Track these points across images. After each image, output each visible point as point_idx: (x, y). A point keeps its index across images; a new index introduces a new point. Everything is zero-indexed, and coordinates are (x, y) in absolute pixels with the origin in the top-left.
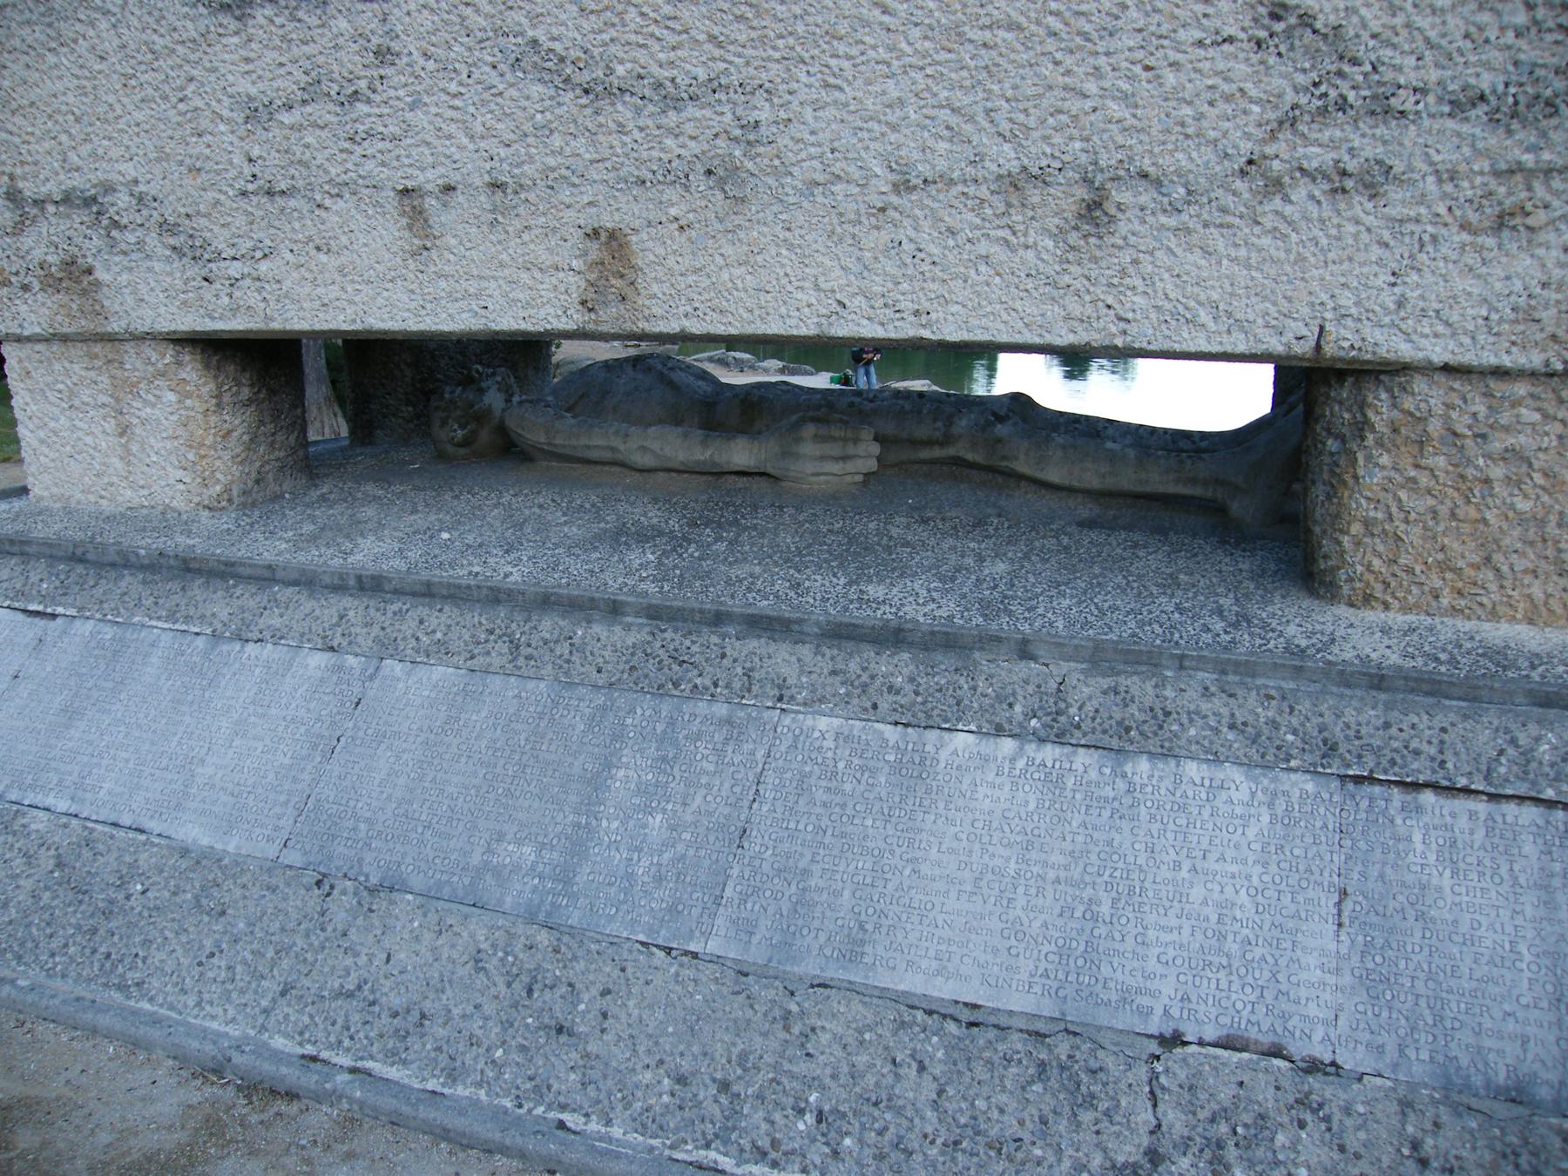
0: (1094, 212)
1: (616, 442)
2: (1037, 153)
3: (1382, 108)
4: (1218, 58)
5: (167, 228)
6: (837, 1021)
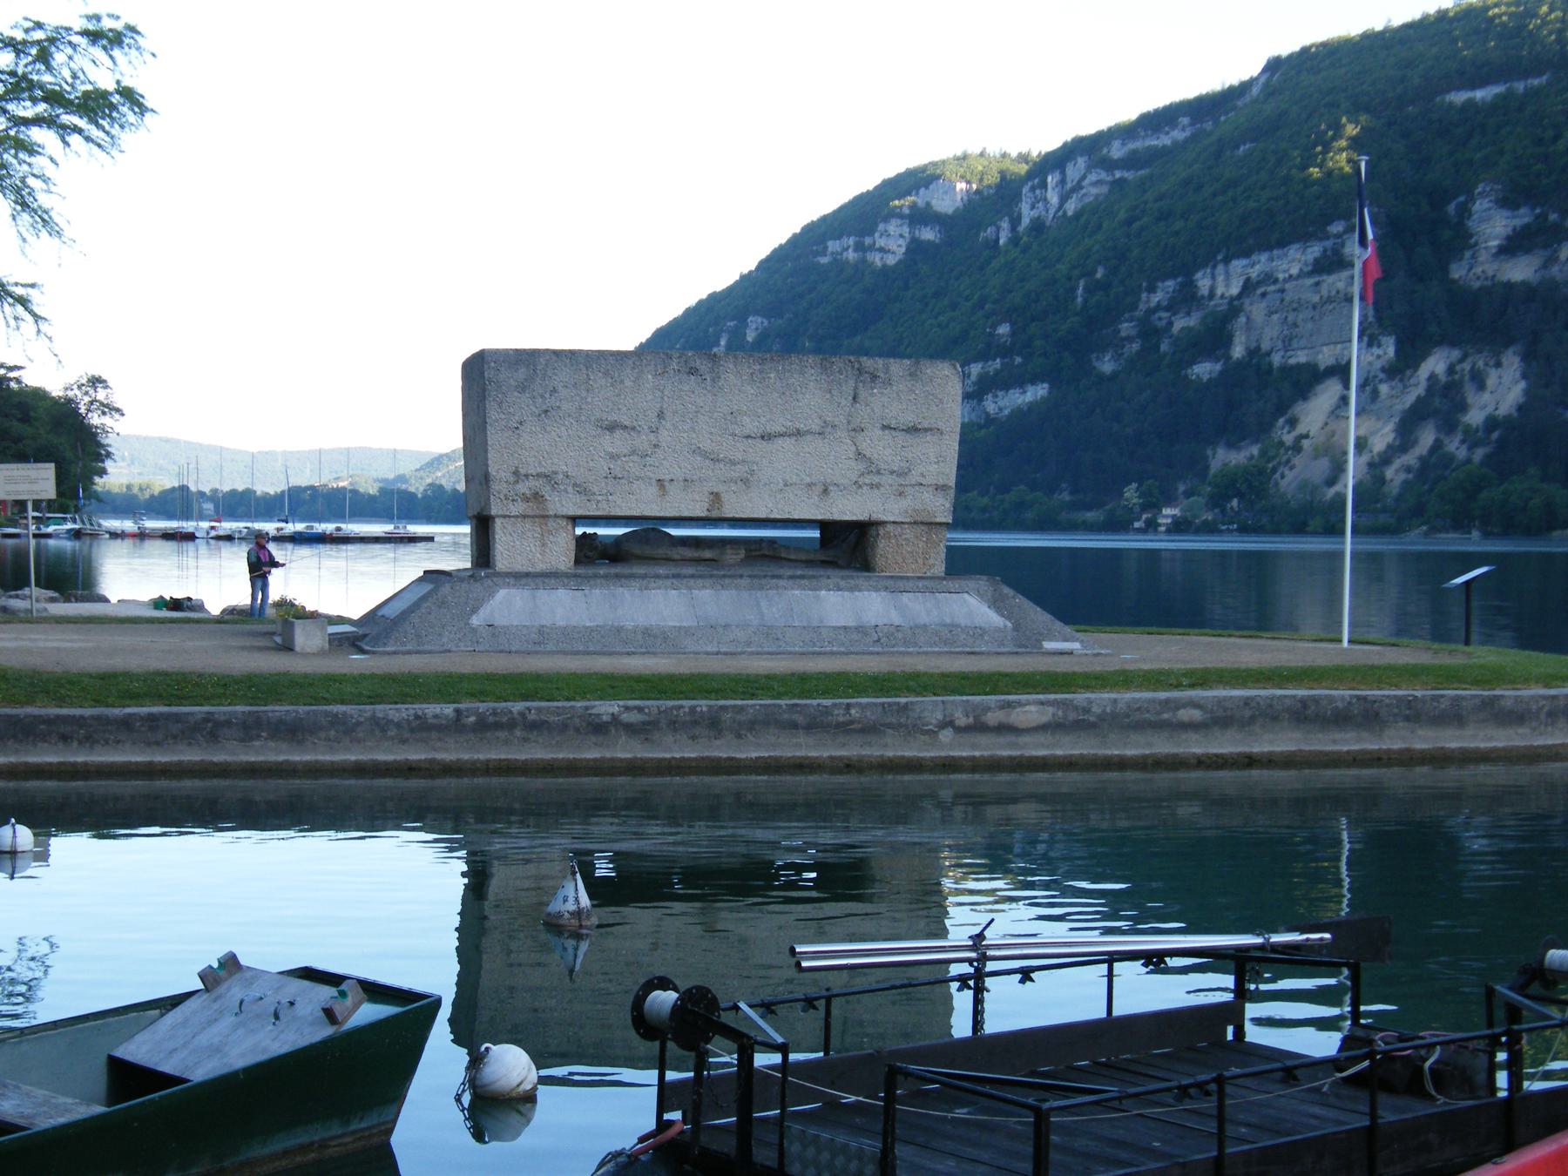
0: (826, 491)
3: (878, 472)
5: (575, 485)
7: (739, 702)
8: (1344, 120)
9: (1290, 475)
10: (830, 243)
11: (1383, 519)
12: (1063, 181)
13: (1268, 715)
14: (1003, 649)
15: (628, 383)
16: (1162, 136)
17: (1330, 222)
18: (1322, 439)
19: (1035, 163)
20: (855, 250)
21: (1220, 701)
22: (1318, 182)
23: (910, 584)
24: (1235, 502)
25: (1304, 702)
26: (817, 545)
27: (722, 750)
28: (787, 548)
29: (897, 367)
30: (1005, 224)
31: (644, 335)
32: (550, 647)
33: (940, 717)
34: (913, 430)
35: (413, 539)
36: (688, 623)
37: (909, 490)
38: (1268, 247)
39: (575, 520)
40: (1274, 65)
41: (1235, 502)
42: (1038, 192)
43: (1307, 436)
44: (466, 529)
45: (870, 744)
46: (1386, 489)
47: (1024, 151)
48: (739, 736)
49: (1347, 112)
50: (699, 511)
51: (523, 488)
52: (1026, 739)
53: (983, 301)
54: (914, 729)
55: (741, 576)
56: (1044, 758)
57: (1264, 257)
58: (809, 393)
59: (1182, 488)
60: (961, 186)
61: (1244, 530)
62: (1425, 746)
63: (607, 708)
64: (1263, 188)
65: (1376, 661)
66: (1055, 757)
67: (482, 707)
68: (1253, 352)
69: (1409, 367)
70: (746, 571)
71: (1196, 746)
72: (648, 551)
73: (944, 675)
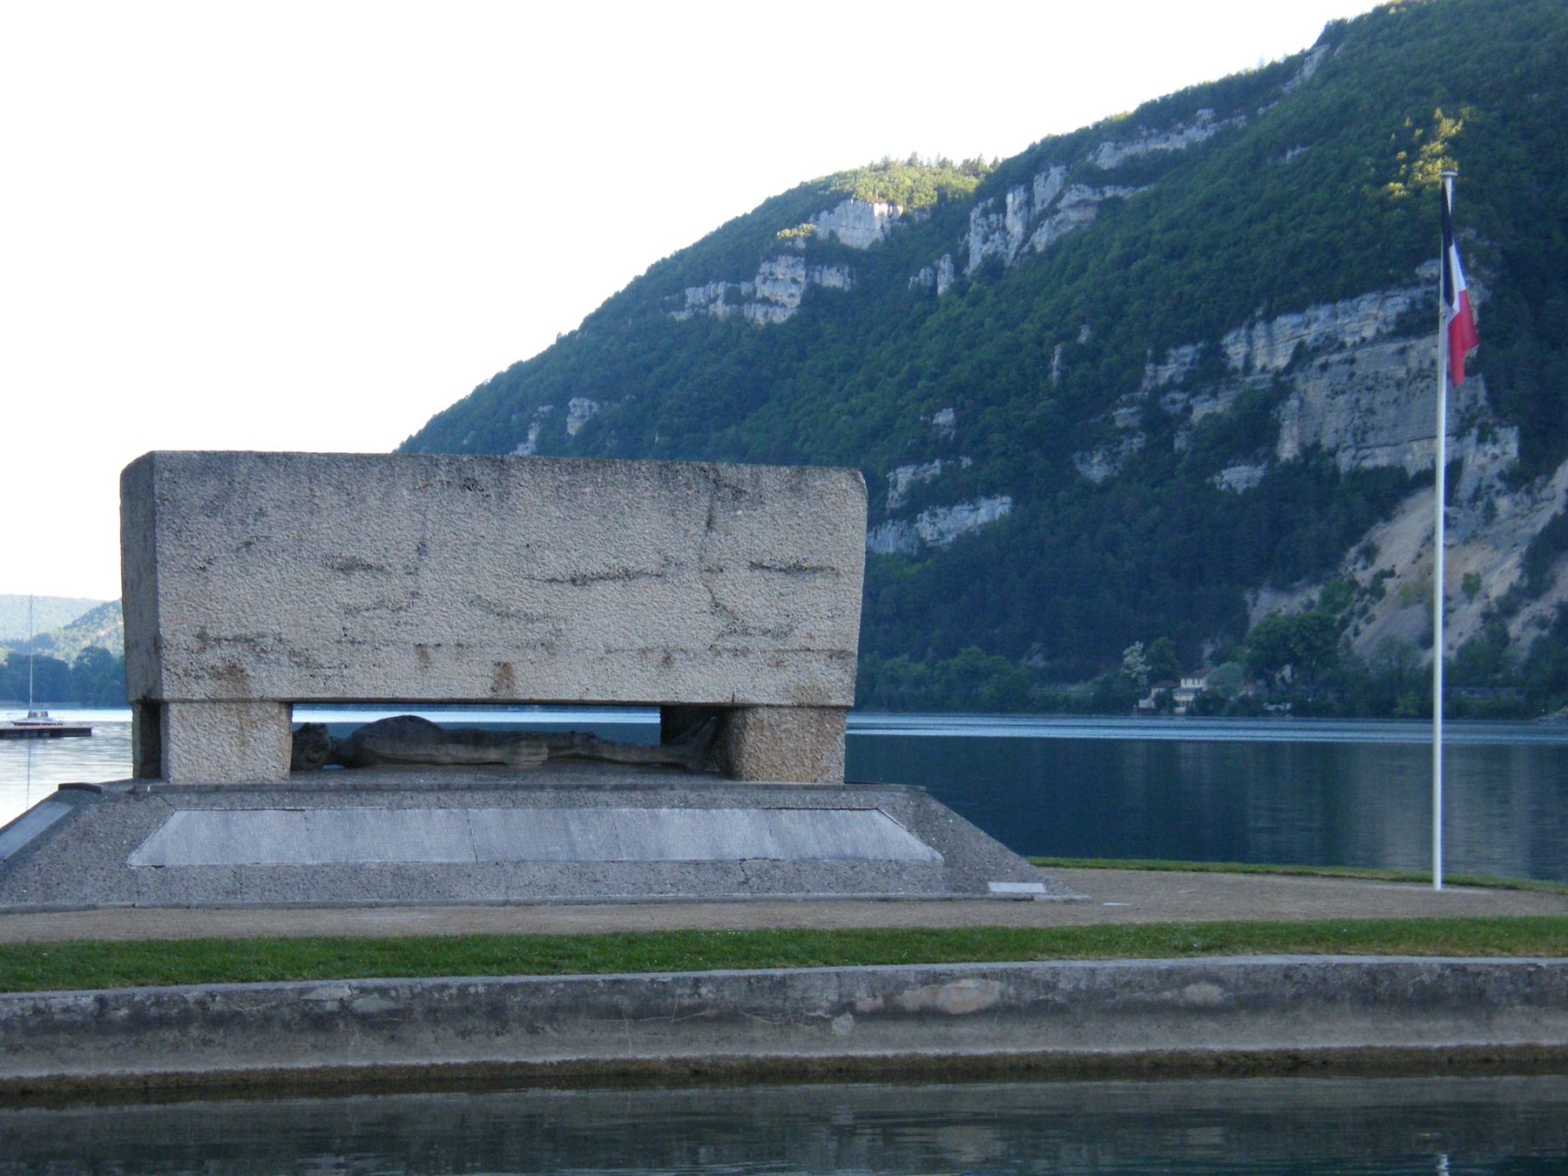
0: (667, 660)
1: (433, 752)
2: (650, 643)
3: (745, 632)
4: (702, 617)
5: (292, 653)
6: (665, 869)
7: (534, 979)
8: (1438, 113)
9: (1367, 631)
10: (689, 291)
11: (1508, 696)
12: (1029, 203)
13: (1317, 994)
14: (930, 894)
15: (373, 501)
16: (1174, 137)
17: (1419, 262)
18: (1414, 578)
19: (988, 176)
20: (726, 302)
21: (1248, 972)
22: (1401, 202)
23: (792, 798)
24: (1287, 671)
25: (1372, 973)
26: (657, 740)
27: (507, 1051)
28: (612, 744)
29: (772, 478)
30: (946, 264)
31: (415, 425)
32: (252, 897)
33: (834, 997)
34: (796, 570)
35: (58, 733)
36: (464, 857)
37: (791, 659)
38: (1329, 298)
39: (290, 705)
40: (1336, 33)
41: (1287, 671)
42: (993, 217)
43: (1391, 574)
44: (127, 716)
45: (729, 1040)
46: (1510, 651)
47: (973, 157)
48: (533, 1030)
49: (1442, 102)
50: (480, 691)
51: (213, 658)
52: (964, 1029)
53: (914, 376)
54: (793, 1017)
55: (542, 788)
56: (989, 1060)
57: (1323, 312)
58: (641, 517)
59: (1208, 650)
60: (881, 209)
61: (1302, 711)
62: (1555, 1042)
63: (332, 991)
64: (1321, 212)
65: (1481, 912)
66: (1005, 1057)
67: (140, 993)
68: (1311, 451)
69: (1538, 473)
70: (549, 780)
71: (1214, 1040)
72: (401, 750)
73: (839, 934)
